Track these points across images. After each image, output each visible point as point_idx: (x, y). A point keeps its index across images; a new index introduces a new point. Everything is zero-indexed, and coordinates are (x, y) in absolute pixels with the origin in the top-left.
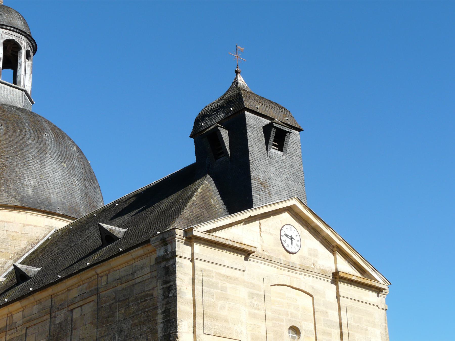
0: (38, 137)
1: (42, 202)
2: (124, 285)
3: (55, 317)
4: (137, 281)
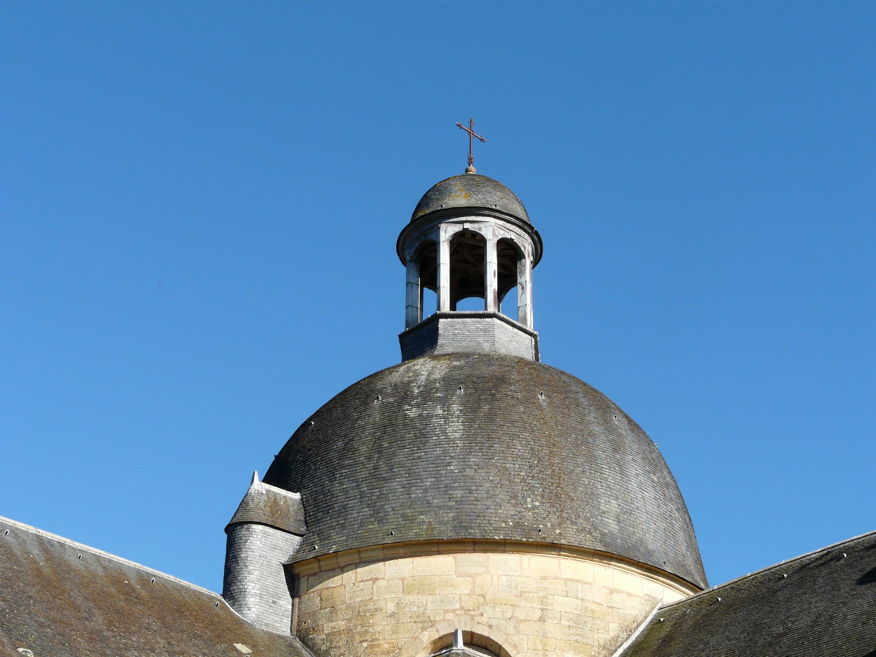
0: (605, 420)
1: (635, 547)
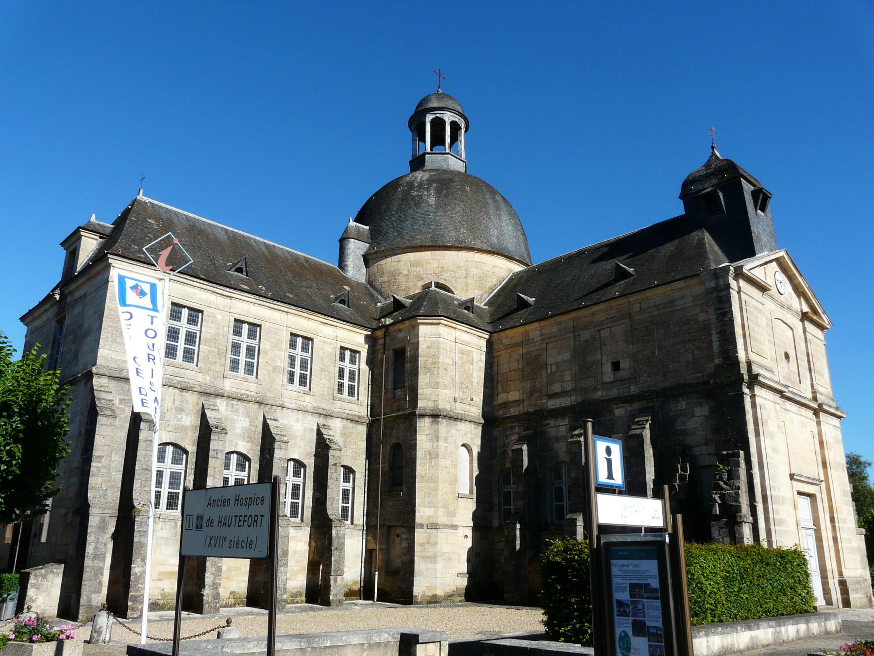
2: (661, 312)
3: (579, 335)
4: (677, 308)
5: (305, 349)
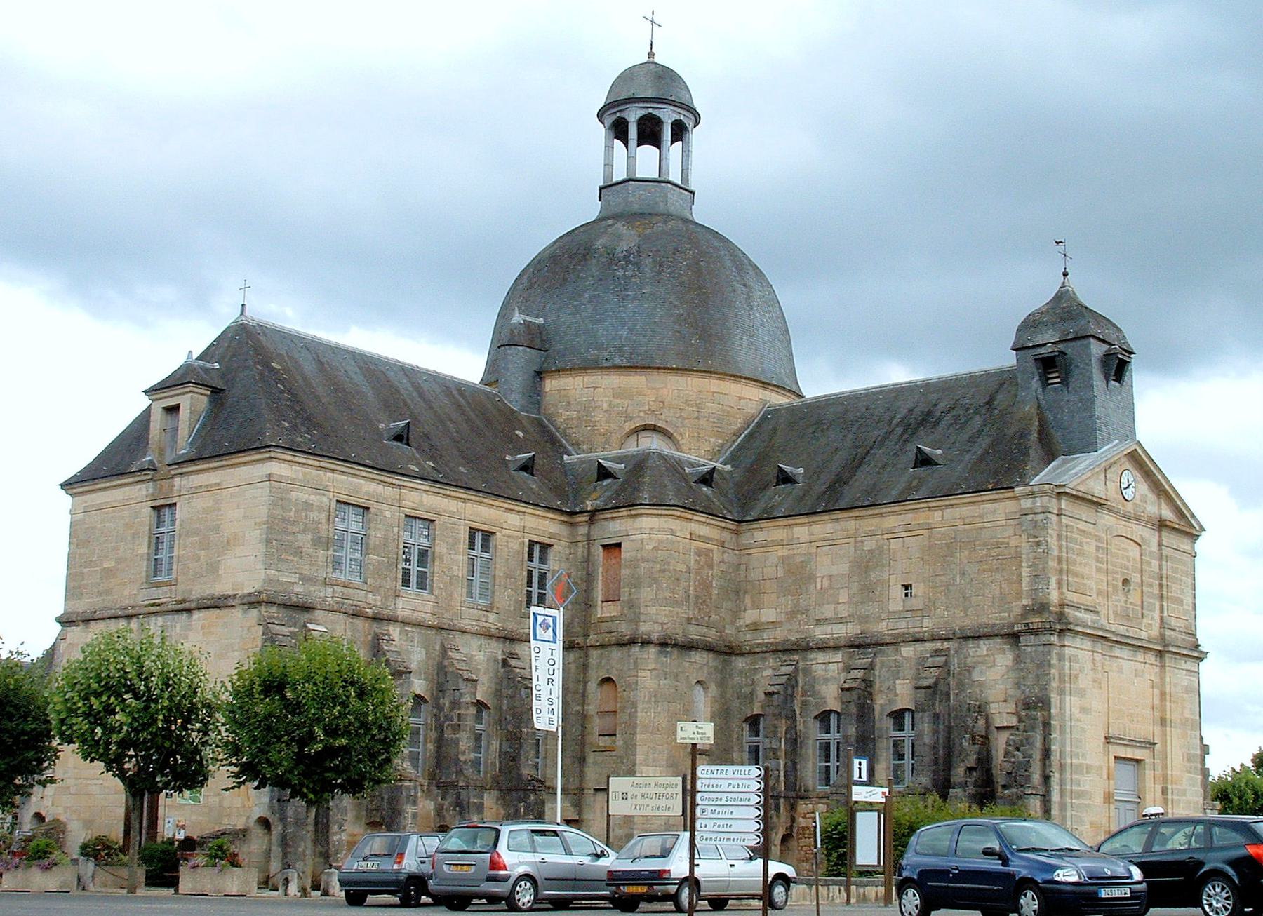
5: (485, 548)
